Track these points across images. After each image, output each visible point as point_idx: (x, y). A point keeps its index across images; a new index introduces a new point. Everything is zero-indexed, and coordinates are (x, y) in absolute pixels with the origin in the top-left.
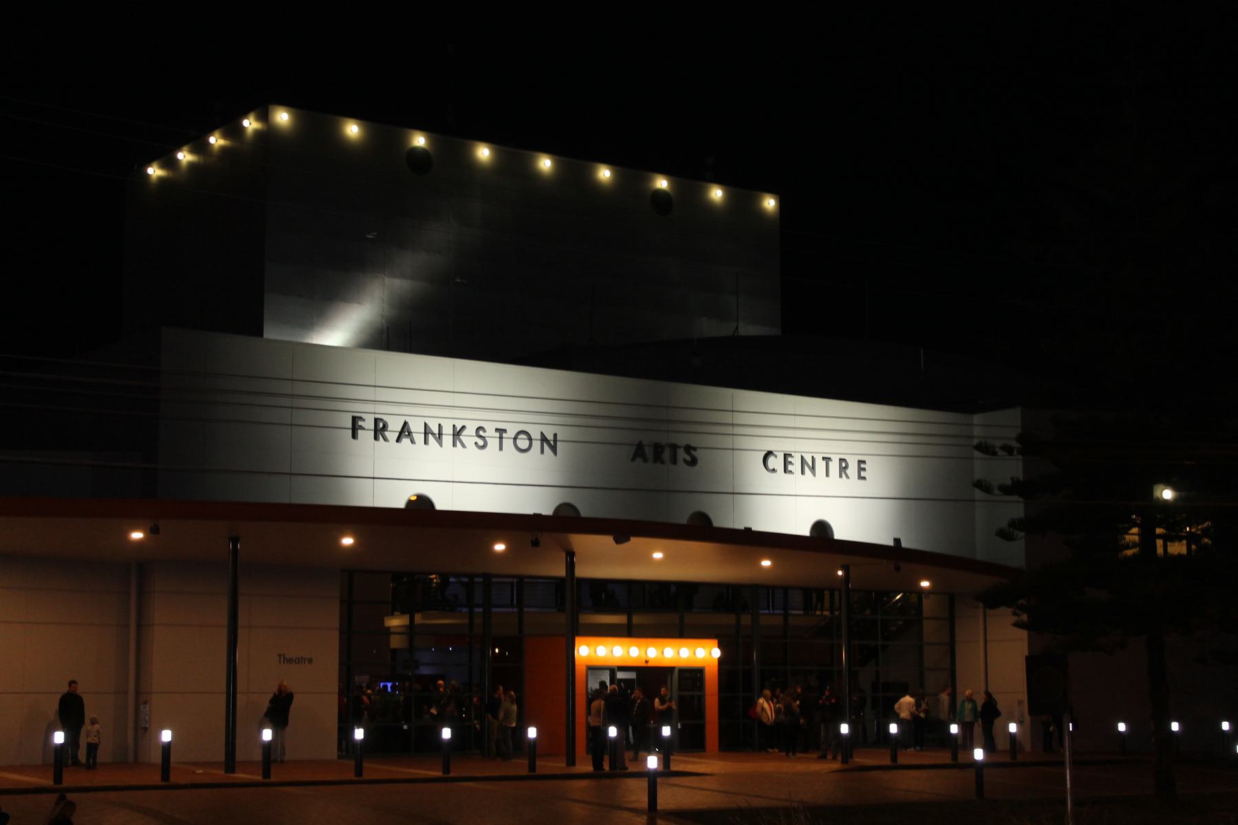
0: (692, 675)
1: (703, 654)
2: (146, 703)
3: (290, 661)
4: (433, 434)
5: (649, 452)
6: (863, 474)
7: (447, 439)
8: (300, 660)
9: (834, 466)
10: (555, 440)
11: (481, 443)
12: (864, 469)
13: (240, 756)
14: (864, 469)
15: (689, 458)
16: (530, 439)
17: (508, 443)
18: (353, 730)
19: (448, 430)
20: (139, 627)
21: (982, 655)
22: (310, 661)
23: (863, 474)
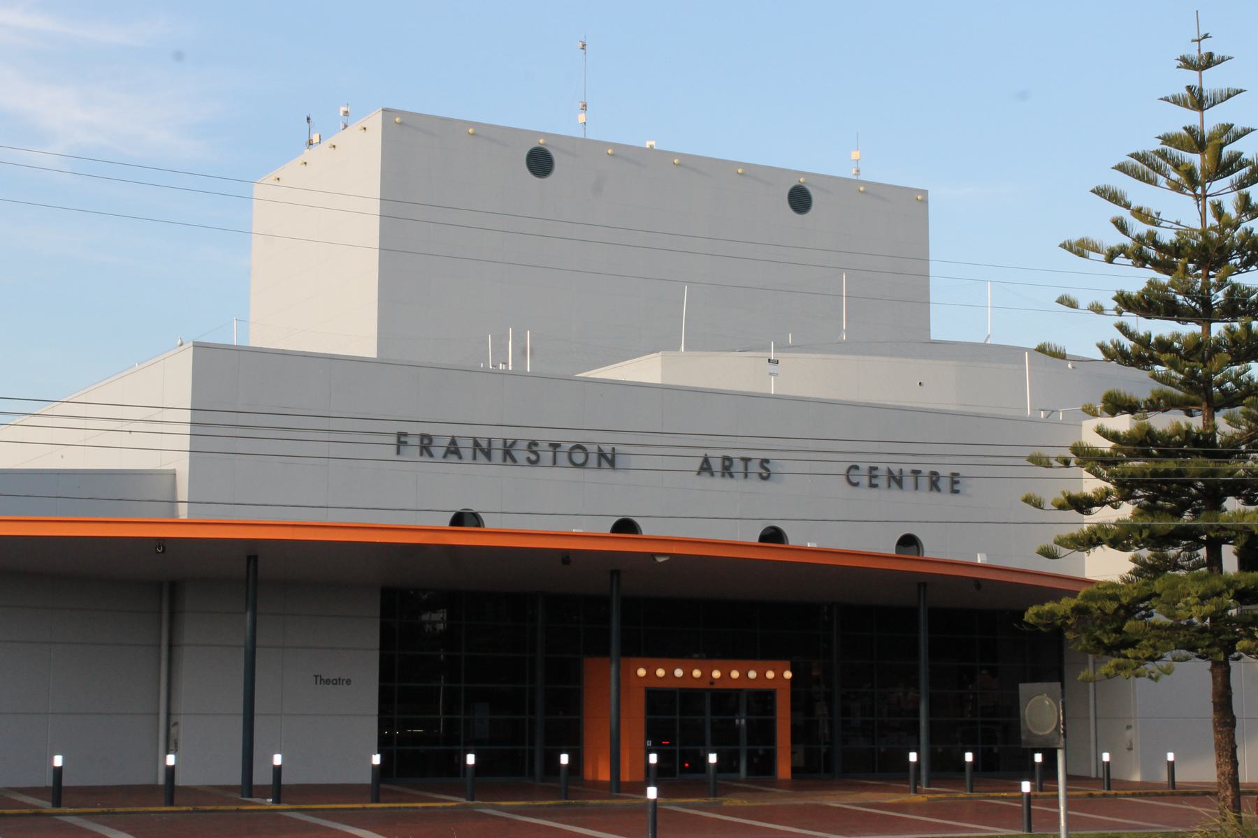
0: (763, 699)
1: (777, 675)
2: (176, 724)
3: (327, 682)
4: (482, 450)
5: (716, 465)
6: (875, 481)
7: (497, 455)
8: (338, 681)
9: (924, 482)
10: (613, 455)
11: (533, 457)
12: (875, 477)
13: (257, 781)
14: (875, 477)
15: (533, 457)
16: (570, 454)
17: (562, 458)
18: (1013, 708)
19: (498, 445)
20: (171, 646)
21: (613, 709)
22: (349, 682)
23: (875, 481)
